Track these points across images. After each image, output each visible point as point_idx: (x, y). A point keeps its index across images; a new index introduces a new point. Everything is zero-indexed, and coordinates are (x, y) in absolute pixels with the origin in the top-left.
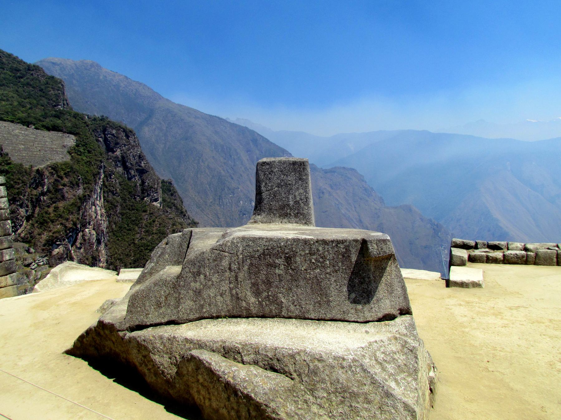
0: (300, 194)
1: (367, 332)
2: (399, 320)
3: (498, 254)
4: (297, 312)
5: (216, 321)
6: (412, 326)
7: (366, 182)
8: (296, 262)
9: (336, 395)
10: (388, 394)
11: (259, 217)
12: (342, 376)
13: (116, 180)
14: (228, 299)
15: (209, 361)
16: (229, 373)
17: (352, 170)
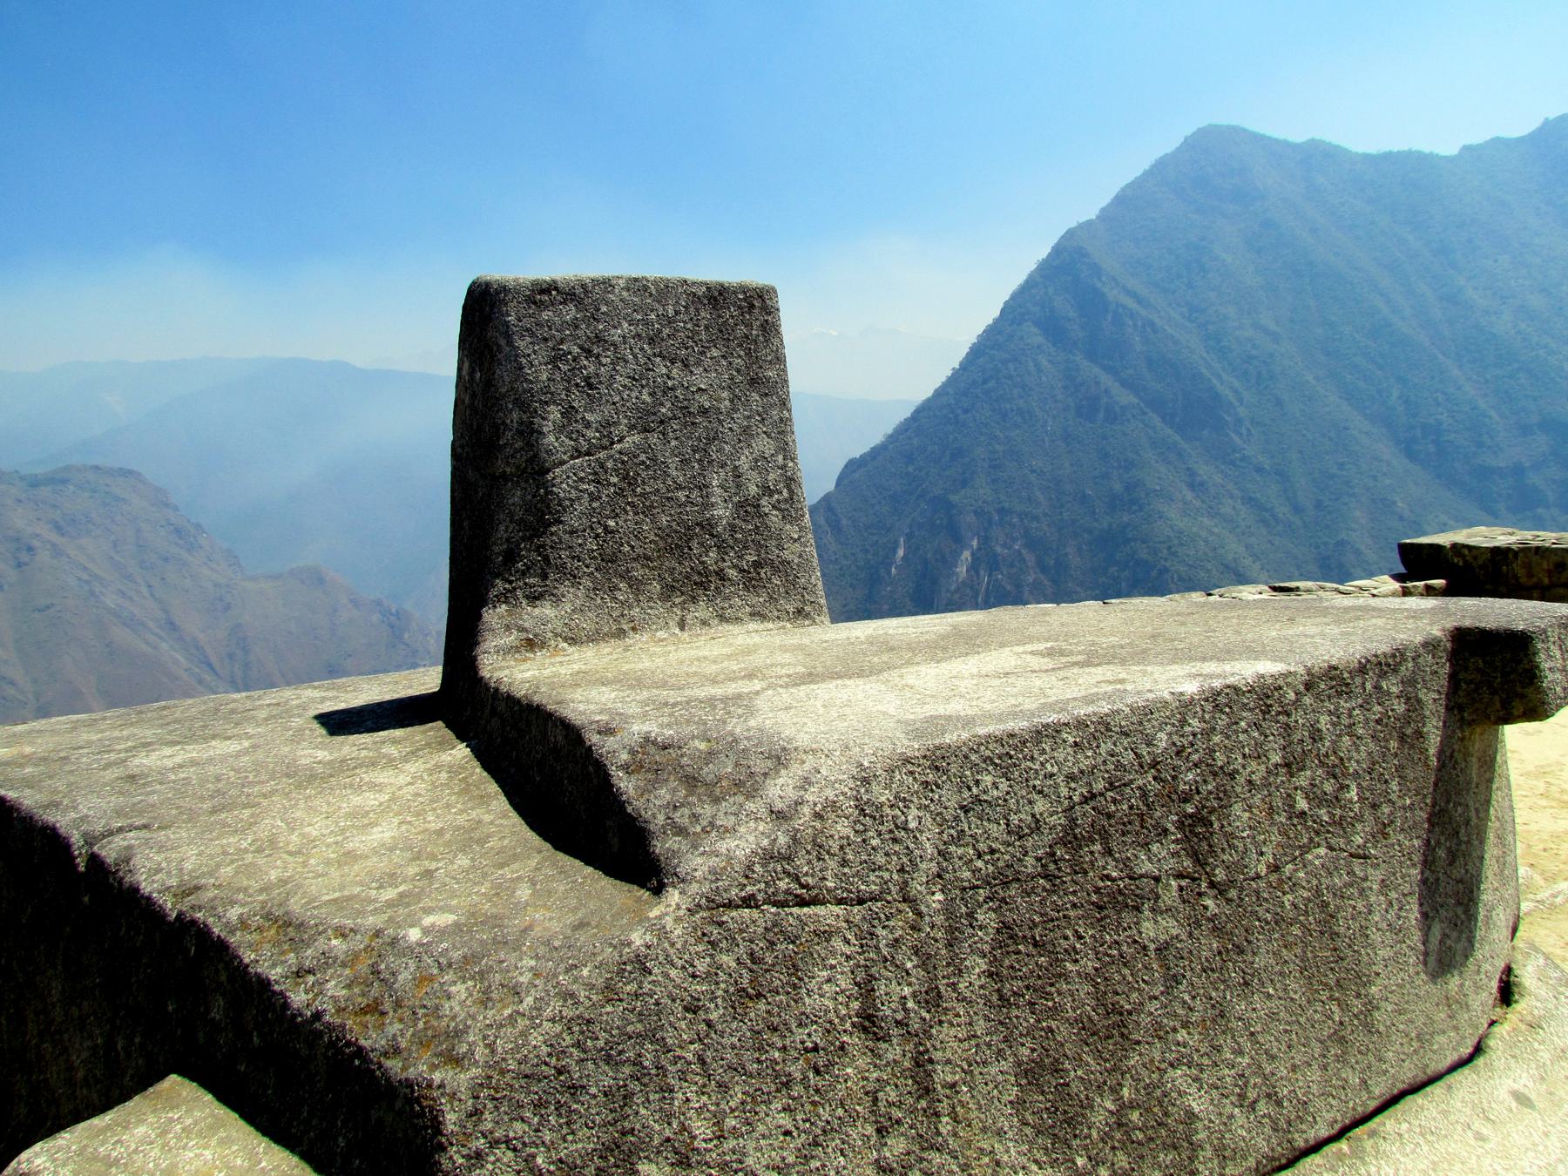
0: (760, 463)
7: (176, 509)
11: (546, 610)
17: (126, 473)
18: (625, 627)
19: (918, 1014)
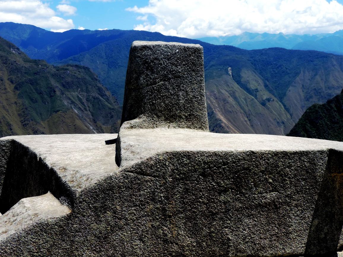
18: (155, 126)
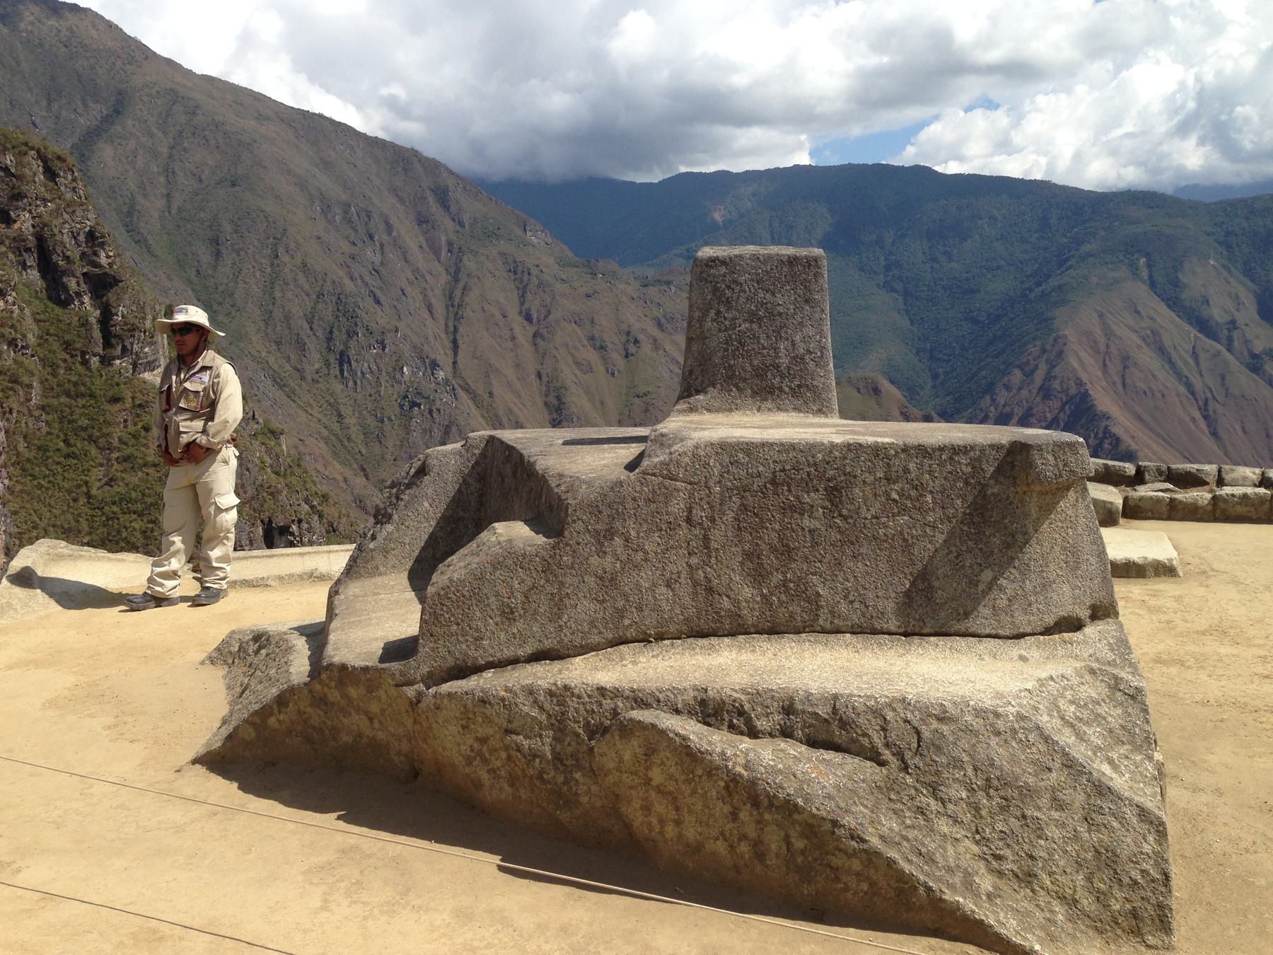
1: (1023, 658)
2: (1091, 630)
3: (1201, 496)
4: (855, 618)
5: (656, 648)
6: (1122, 645)
8: (852, 501)
9: (988, 794)
10: (1101, 789)
11: (701, 397)
12: (998, 752)
13: (22, 310)
14: (684, 589)
15: (682, 732)
16: (735, 755)
19: (707, 523)
